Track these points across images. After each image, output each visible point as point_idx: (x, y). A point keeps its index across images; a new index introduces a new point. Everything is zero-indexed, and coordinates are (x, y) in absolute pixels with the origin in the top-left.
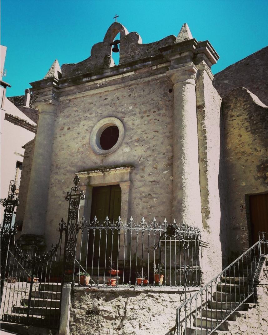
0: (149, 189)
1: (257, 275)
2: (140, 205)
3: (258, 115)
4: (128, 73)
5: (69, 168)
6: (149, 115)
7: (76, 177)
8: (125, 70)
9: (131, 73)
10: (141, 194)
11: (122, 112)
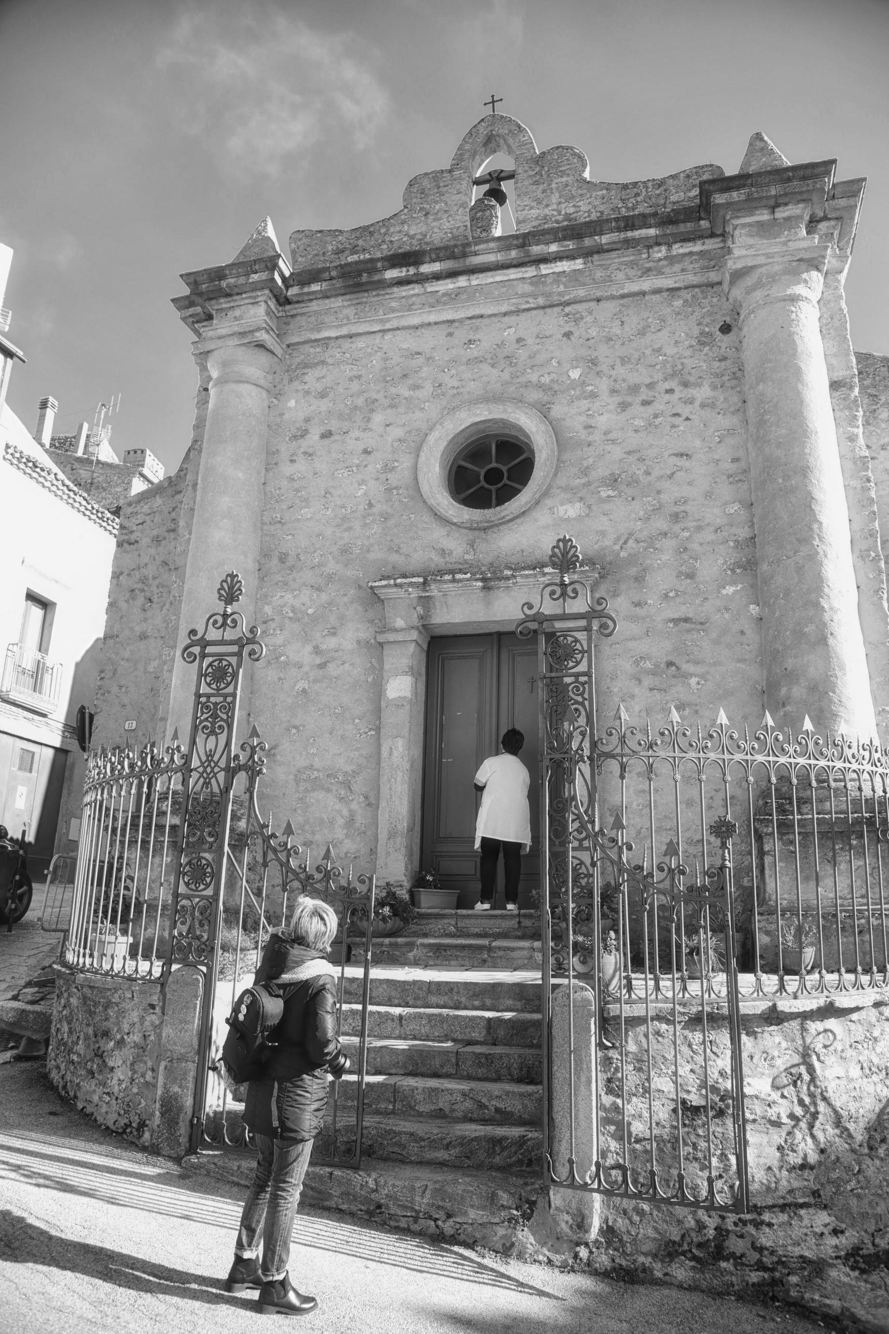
2: (637, 699)
4: (559, 264)
5: (332, 567)
6: (652, 401)
7: (559, 540)
8: (553, 248)
9: (572, 262)
10: (637, 663)
11: (540, 386)
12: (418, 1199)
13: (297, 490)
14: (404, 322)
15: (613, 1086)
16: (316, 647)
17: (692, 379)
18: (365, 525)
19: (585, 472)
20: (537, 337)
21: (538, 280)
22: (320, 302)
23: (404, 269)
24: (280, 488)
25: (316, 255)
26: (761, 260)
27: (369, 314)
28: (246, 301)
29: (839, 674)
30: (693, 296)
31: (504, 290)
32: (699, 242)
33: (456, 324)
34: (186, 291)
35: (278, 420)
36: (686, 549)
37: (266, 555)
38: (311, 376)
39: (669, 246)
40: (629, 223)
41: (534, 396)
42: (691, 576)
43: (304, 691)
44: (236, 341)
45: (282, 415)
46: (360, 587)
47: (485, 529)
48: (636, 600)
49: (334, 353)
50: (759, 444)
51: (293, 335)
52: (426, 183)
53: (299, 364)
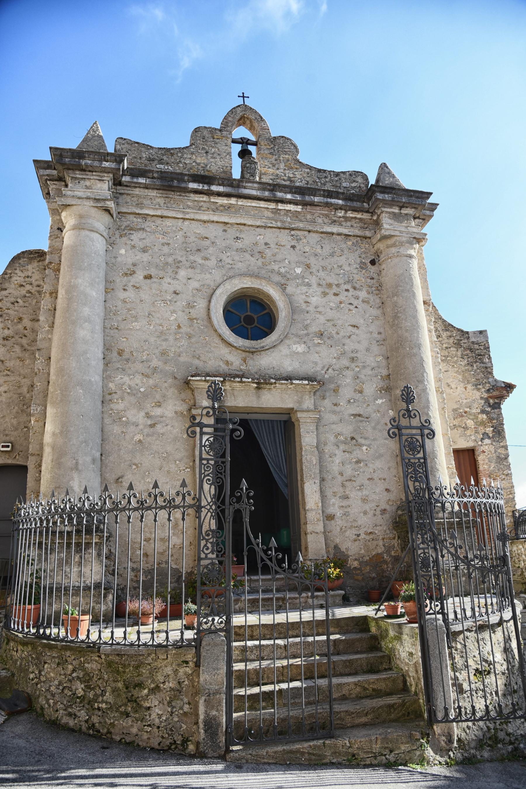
0: (350, 428)
1: (112, 563)
2: (337, 457)
3: (450, 337)
4: (289, 205)
5: (155, 363)
7: (405, 387)
8: (289, 196)
10: (336, 437)
12: (374, 746)
13: (129, 310)
14: (197, 217)
15: (454, 669)
16: (147, 413)
17: (358, 286)
18: (176, 339)
19: (306, 327)
20: (277, 244)
21: (276, 211)
22: (142, 190)
23: (201, 185)
24: (116, 306)
25: (135, 158)
26: (397, 233)
27: (174, 206)
28: (95, 177)
29: (438, 450)
30: (357, 241)
31: (257, 212)
32: (361, 214)
33: (229, 226)
34: (47, 157)
35: (113, 260)
36: (358, 377)
37: (107, 349)
38: (136, 237)
39: (346, 211)
40: (330, 194)
41: (277, 278)
42: (361, 392)
43: (140, 441)
44: (92, 203)
45: (115, 258)
46: (175, 378)
47: (253, 353)
48: (334, 402)
49: (149, 225)
50: (394, 328)
51: (123, 207)
52: (205, 133)
53: (126, 227)
